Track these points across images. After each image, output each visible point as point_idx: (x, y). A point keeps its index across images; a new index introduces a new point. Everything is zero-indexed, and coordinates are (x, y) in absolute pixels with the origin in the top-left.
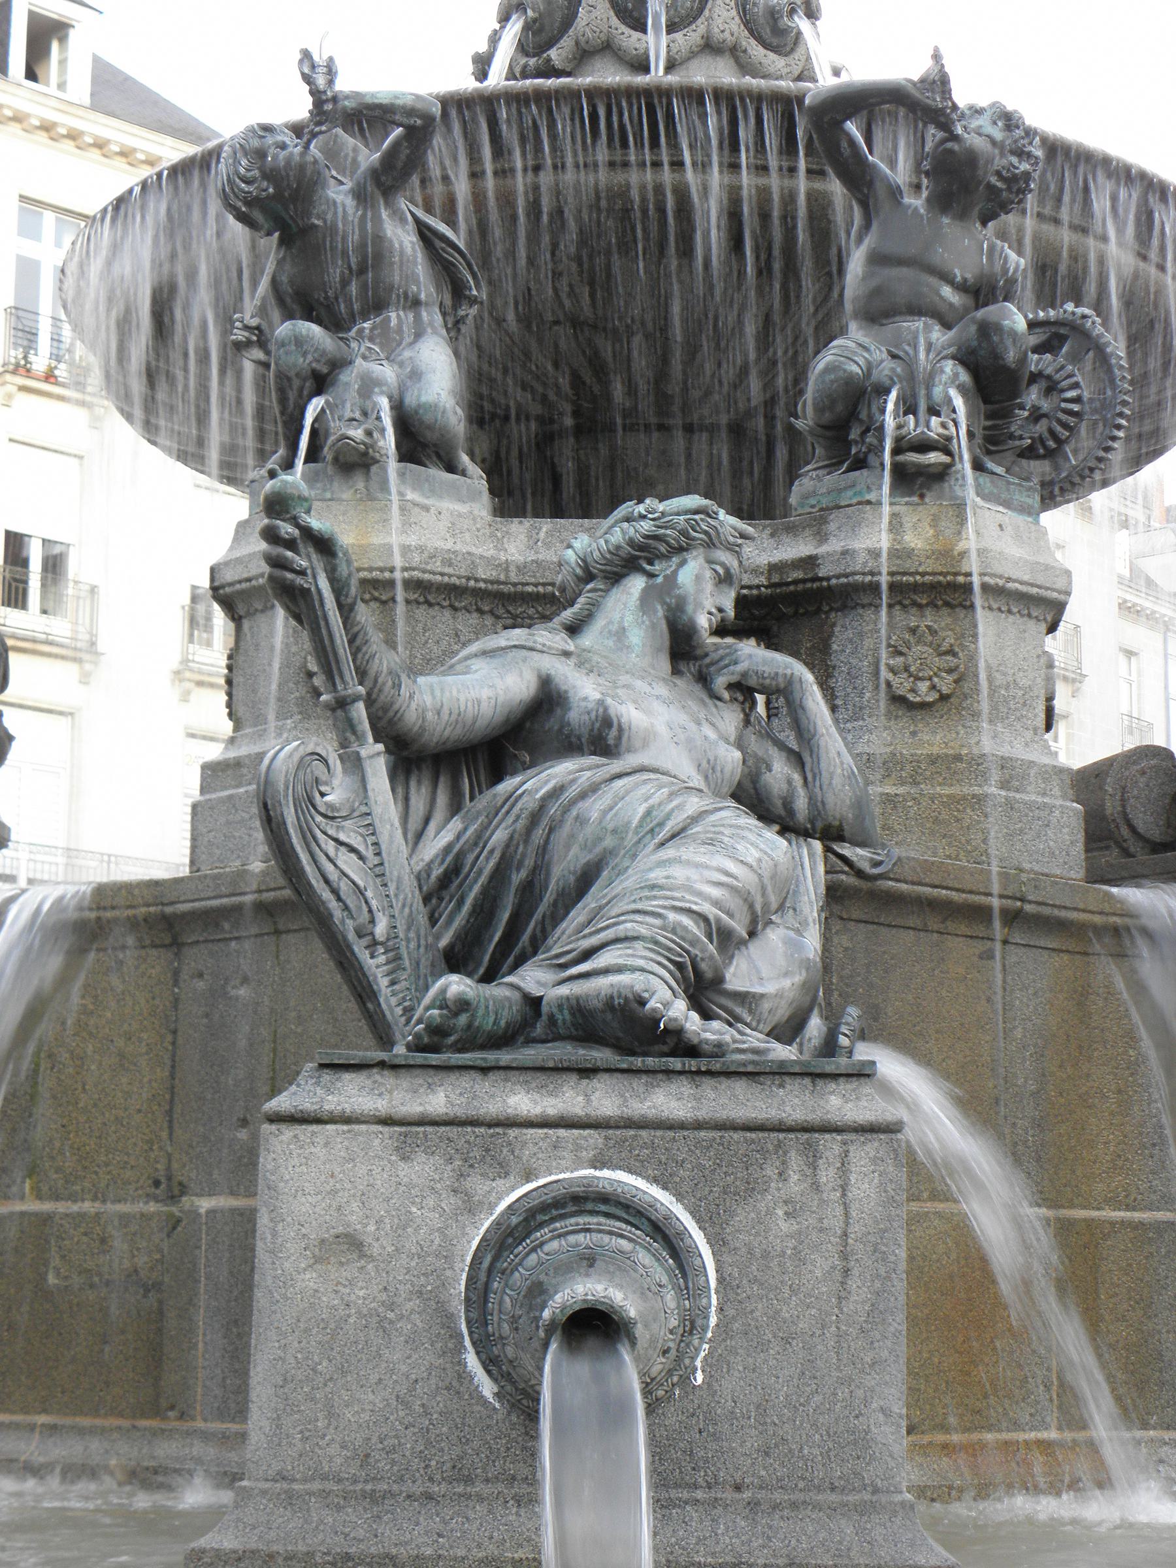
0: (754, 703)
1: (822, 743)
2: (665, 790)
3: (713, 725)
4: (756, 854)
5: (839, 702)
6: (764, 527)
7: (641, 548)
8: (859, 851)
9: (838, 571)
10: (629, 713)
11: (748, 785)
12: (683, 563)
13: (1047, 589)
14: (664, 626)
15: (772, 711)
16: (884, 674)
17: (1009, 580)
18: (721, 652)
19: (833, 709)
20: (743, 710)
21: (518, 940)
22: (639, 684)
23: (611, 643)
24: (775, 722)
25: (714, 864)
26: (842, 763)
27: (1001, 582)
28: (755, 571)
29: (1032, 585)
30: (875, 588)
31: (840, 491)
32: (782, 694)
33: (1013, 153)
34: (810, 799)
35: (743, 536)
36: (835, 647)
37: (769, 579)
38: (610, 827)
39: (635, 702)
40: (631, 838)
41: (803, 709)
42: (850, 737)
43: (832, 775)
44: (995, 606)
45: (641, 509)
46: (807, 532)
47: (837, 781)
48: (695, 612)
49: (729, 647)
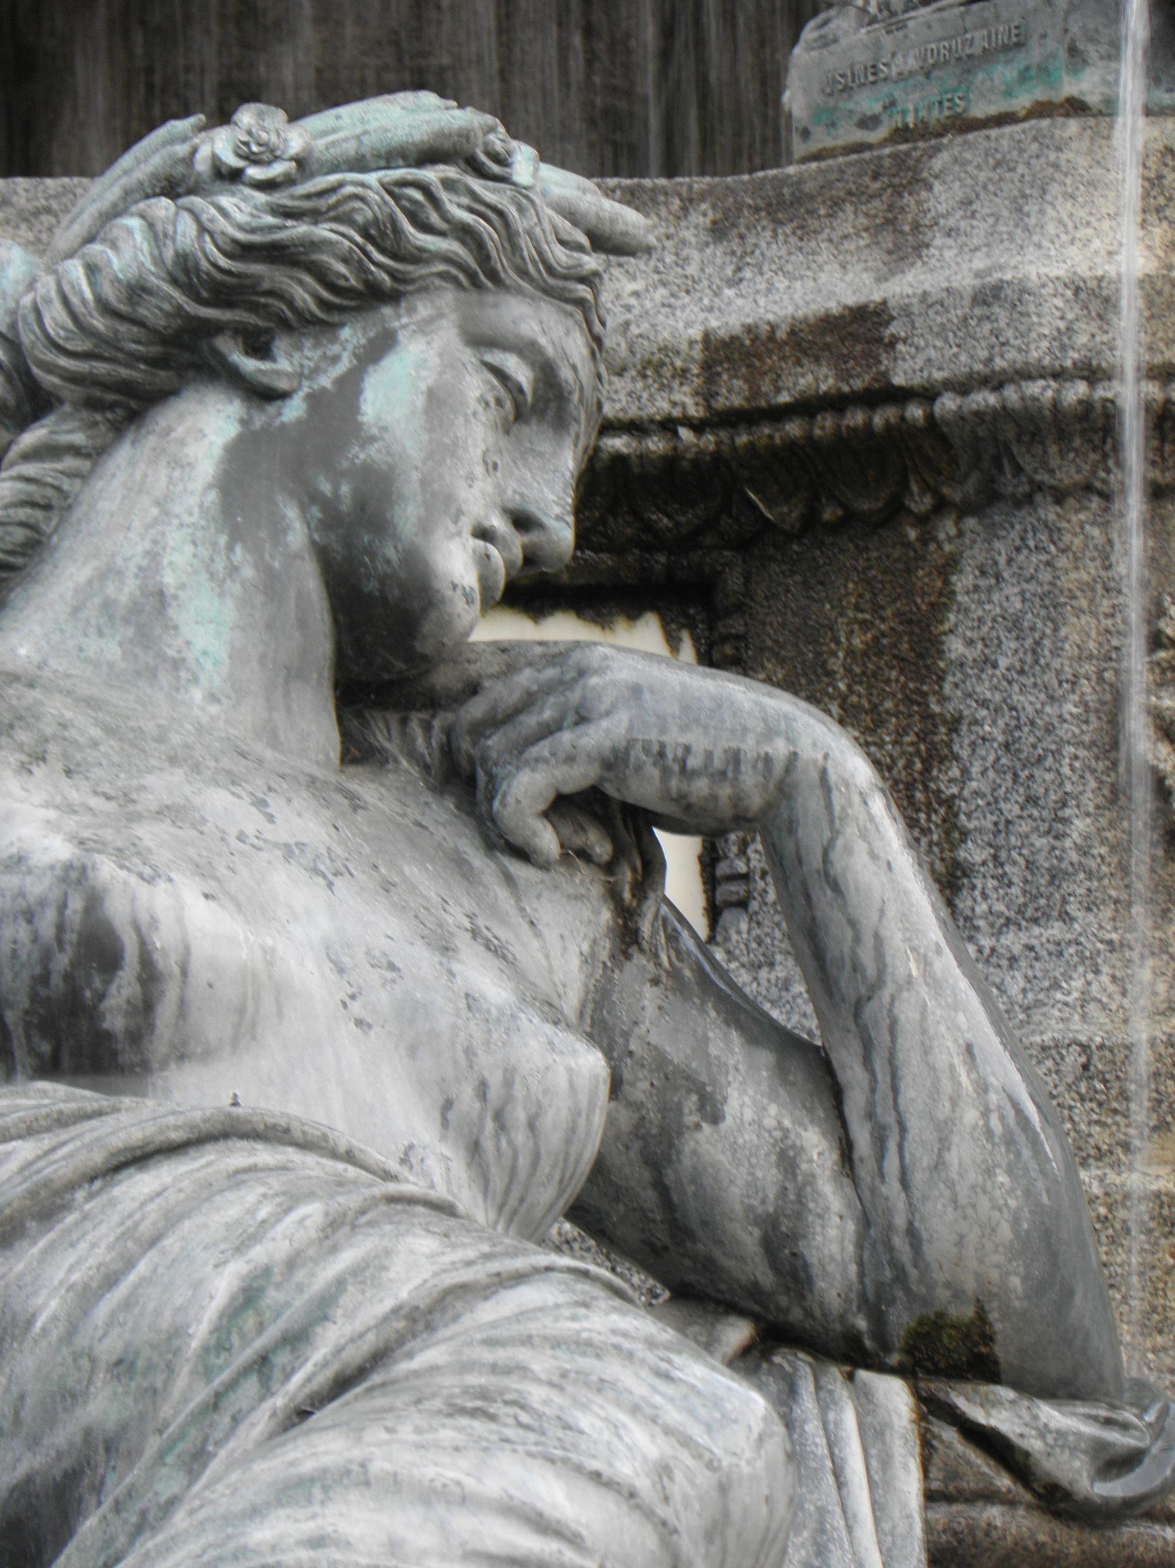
0: (652, 867)
1: (907, 1013)
2: (313, 1212)
3: (497, 951)
4: (647, 1444)
5: (974, 853)
6: (689, 202)
7: (224, 291)
8: (1051, 1415)
9: (965, 362)
10: (182, 913)
11: (632, 1172)
12: (381, 346)
14: (309, 582)
15: (722, 895)
16: (1143, 745)
18: (525, 678)
19: (950, 881)
20: (613, 894)
21: (775, 884)
22: (222, 805)
23: (112, 650)
24: (738, 926)
25: (492, 1487)
26: (983, 1088)
28: (655, 367)
30: (1096, 427)
31: (968, 64)
32: (760, 840)
34: (865, 1221)
35: (603, 241)
36: (956, 647)
37: (707, 395)
38: (110, 1347)
39: (202, 870)
40: (186, 1391)
41: (836, 887)
42: (1015, 984)
43: (944, 1132)
45: (221, 145)
46: (849, 219)
47: (963, 1153)
48: (426, 526)
49: (557, 656)
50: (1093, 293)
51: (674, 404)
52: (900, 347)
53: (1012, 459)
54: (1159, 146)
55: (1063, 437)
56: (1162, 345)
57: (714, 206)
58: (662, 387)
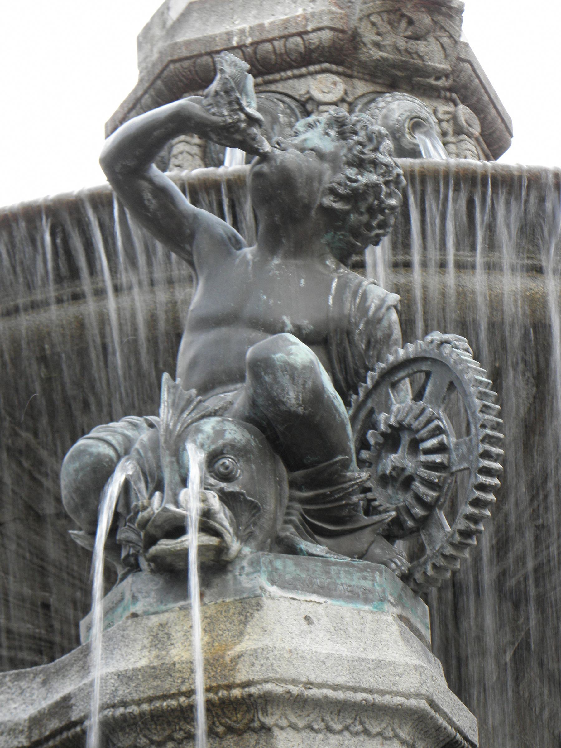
6: (36, 675)
13: (383, 693)
17: (309, 685)
27: (295, 690)
29: (355, 689)
33: (350, 164)
37: (29, 737)
44: (301, 724)
50: (124, 676)
51: (19, 742)
52: (74, 707)
53: (112, 741)
54: (158, 624)
55: (122, 729)
56: (147, 690)
57: (44, 675)
58: (16, 737)
